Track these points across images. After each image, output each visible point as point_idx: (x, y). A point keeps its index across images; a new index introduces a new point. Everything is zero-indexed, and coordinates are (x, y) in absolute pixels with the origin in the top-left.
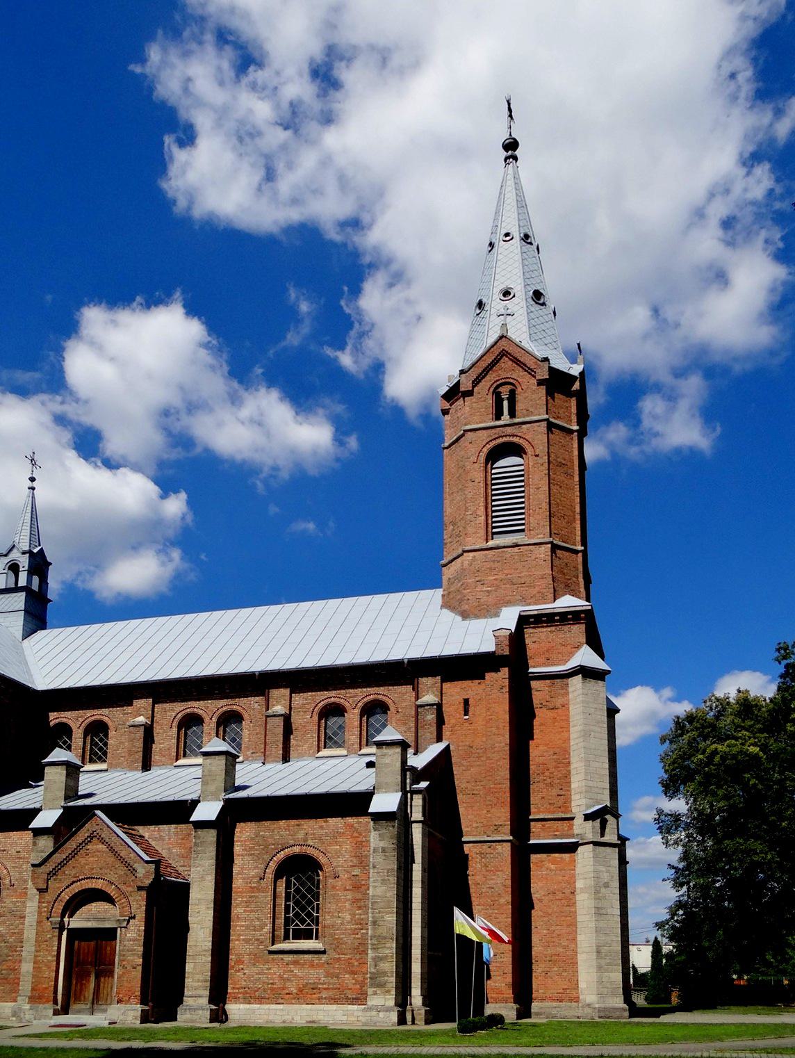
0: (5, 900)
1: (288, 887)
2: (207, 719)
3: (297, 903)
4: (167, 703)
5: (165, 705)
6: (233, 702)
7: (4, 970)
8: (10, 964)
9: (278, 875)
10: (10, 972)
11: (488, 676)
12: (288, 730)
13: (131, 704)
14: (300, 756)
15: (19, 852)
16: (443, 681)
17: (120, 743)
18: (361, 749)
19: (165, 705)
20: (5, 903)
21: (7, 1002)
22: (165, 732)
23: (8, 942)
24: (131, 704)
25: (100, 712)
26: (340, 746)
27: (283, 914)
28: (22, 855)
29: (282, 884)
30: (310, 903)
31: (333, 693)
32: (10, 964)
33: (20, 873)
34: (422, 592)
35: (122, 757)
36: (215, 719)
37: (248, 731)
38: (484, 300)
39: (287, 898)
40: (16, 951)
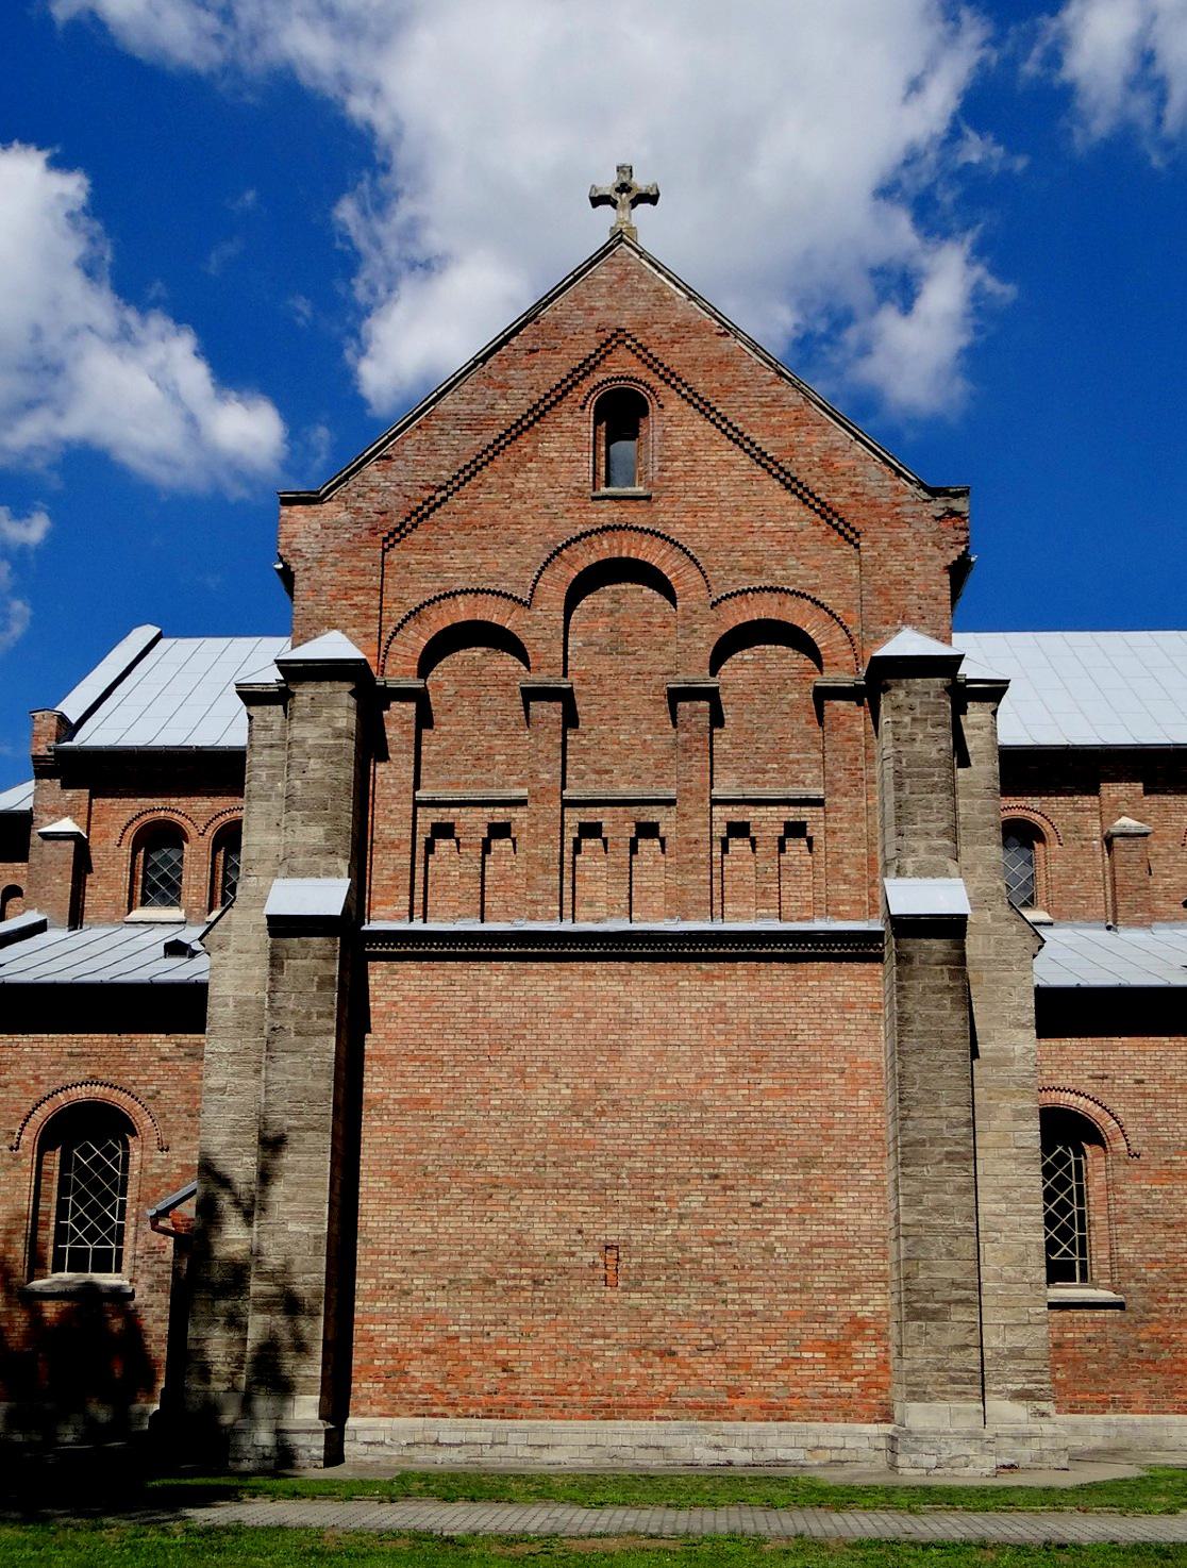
0: (1122, 1187)
1: (65, 1165)
2: (192, 832)
3: (82, 1198)
4: (1170, 794)
5: (1166, 798)
6: (1022, 803)
7: (1146, 1341)
8: (1155, 1328)
9: (46, 1141)
10: (1161, 1347)
11: (1105, 788)
12: (82, 863)
13: (1095, 792)
14: (99, 922)
15: (1140, 1082)
16: (92, 796)
17: (1075, 868)
18: (130, 910)
19: (1165, 797)
20: (1123, 1192)
21: (1164, 1413)
22: (1171, 852)
23: (1145, 1281)
24: (1095, 792)
25: (1022, 803)
26: (172, 904)
27: (53, 1219)
28: (1149, 1088)
29: (54, 1159)
30: (107, 1199)
31: (157, 802)
32: (1155, 1328)
33: (1151, 1128)
34: (266, 640)
35: (1083, 898)
36: (210, 833)
37: (1051, 858)
38: (621, 162)
39: (64, 1188)
40: (1167, 1301)
